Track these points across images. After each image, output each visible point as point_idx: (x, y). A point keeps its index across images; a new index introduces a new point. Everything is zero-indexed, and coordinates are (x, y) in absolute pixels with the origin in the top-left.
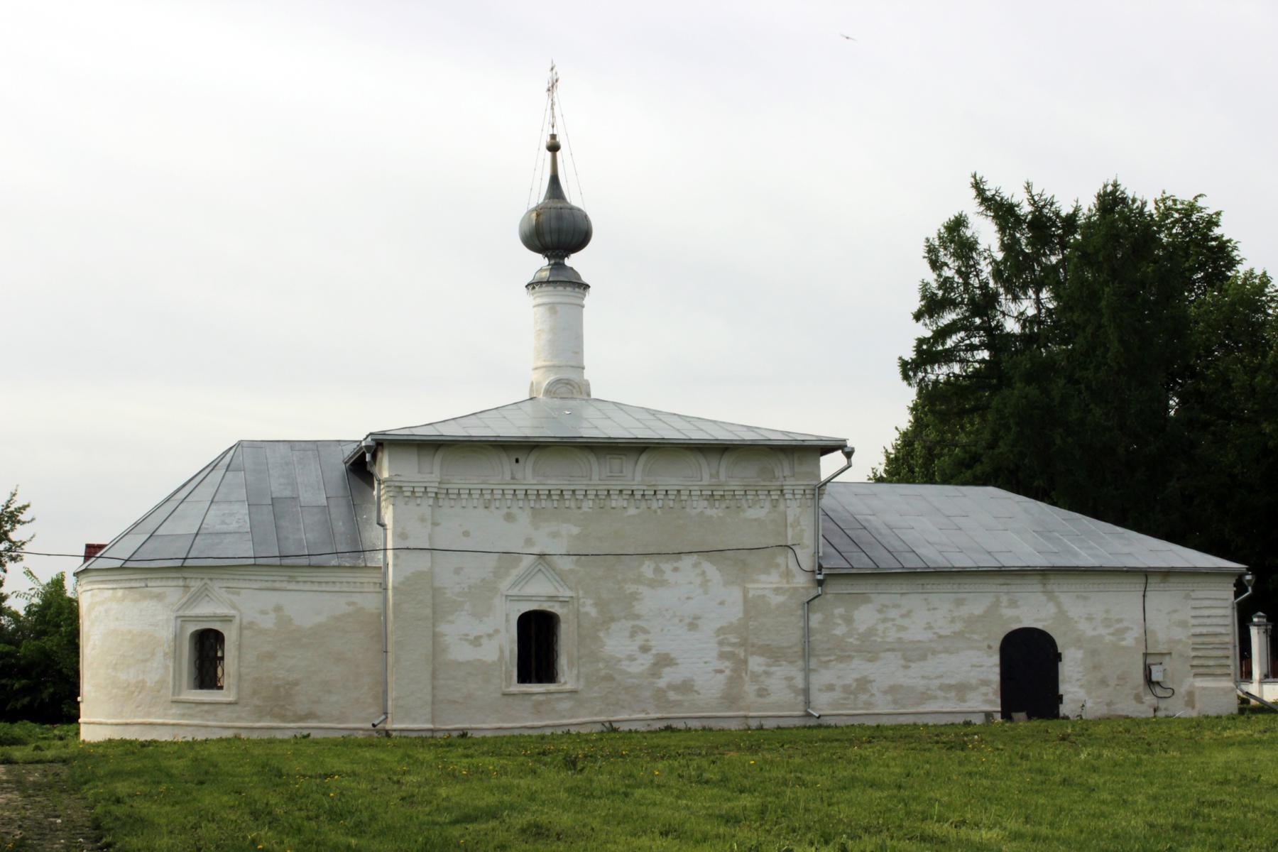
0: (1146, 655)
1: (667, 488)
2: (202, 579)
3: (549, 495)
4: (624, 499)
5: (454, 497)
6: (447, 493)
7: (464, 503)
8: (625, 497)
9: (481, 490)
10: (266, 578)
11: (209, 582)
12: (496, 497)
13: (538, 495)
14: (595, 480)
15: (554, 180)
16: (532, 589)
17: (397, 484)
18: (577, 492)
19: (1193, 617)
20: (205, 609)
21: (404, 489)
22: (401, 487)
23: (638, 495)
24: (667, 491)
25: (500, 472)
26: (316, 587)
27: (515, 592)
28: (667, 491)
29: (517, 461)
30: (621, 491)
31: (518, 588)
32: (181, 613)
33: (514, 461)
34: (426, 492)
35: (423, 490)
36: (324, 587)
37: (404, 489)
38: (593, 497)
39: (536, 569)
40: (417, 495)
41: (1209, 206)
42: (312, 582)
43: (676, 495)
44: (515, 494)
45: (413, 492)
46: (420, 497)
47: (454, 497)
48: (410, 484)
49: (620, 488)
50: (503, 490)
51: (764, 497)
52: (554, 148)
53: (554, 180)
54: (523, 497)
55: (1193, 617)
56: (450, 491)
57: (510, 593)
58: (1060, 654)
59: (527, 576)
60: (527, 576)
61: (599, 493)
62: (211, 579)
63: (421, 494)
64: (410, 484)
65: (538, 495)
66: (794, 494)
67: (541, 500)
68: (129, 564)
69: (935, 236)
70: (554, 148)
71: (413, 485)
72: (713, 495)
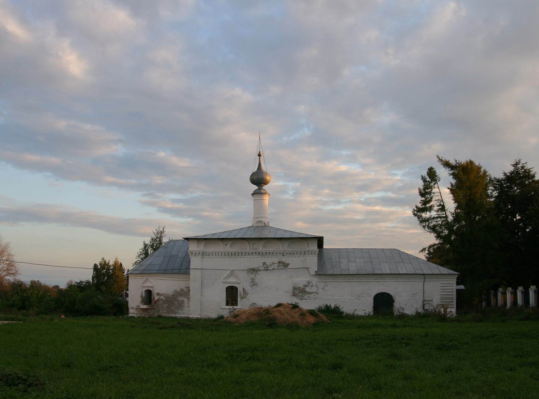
0: (424, 301)
1: (269, 252)
2: (147, 276)
3: (235, 254)
4: (260, 255)
5: (208, 255)
6: (206, 254)
7: (211, 256)
8: (257, 254)
9: (216, 253)
10: (161, 276)
11: (148, 277)
12: (220, 255)
13: (232, 254)
14: (248, 250)
15: (260, 164)
16: (229, 280)
17: (191, 252)
18: (243, 253)
19: (441, 289)
20: (148, 284)
21: (193, 253)
22: (192, 252)
23: (261, 254)
24: (269, 253)
25: (220, 248)
26: (173, 279)
27: (225, 281)
28: (269, 253)
29: (226, 245)
30: (256, 253)
31: (226, 280)
32: (142, 285)
33: (225, 245)
34: (199, 254)
35: (198, 253)
36: (175, 279)
37: (193, 253)
38: (275, 254)
39: (231, 275)
40: (197, 254)
41: (448, 160)
42: (172, 278)
43: (300, 253)
44: (225, 254)
45: (196, 254)
46: (198, 255)
47: (208, 255)
48: (293, 251)
49: (255, 252)
50: (222, 253)
51: (296, 254)
52: (259, 155)
53: (260, 164)
54: (227, 255)
55: (441, 289)
56: (207, 253)
57: (223, 281)
58: (394, 300)
59: (228, 276)
60: (228, 276)
61: (249, 253)
62: (149, 277)
63: (198, 254)
64: (293, 251)
65: (232, 254)
66: (308, 253)
67: (229, 256)
68: (144, 272)
69: (426, 174)
70: (259, 155)
71: (293, 251)
72: (290, 253)
